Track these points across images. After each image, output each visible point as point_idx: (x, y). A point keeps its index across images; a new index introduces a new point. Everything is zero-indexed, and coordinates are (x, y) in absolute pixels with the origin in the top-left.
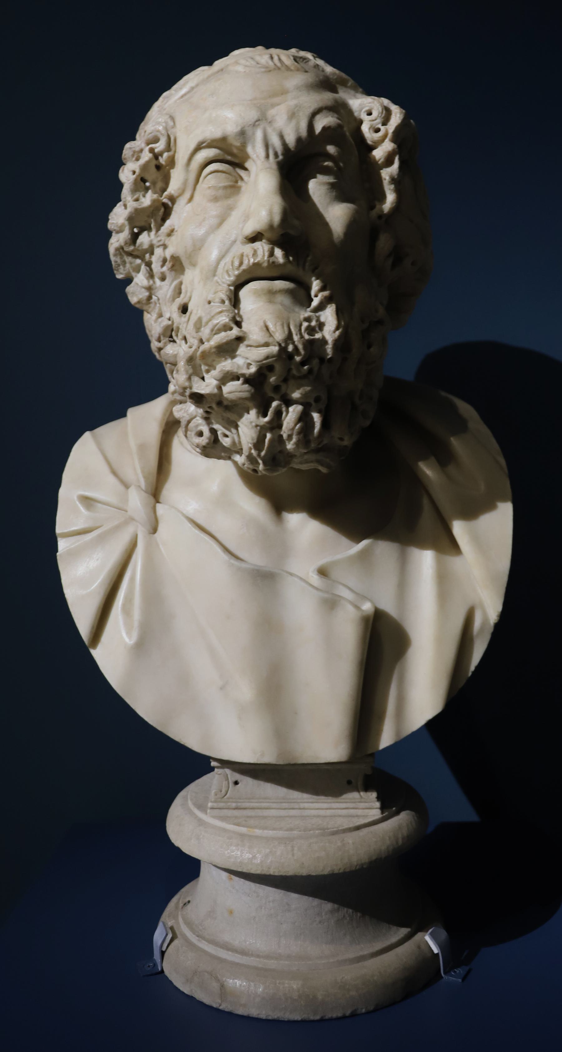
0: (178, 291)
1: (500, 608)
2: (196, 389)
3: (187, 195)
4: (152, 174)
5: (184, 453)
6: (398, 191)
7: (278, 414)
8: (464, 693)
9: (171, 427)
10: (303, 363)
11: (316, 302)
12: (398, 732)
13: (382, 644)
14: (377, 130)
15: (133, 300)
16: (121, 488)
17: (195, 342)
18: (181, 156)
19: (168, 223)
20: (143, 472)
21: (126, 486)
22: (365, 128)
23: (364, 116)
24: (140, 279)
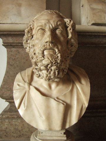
0: (34, 50)
1: (88, 105)
2: (36, 68)
3: (36, 34)
4: (30, 30)
5: (35, 77)
6: (72, 34)
7: (50, 72)
8: (82, 120)
9: (33, 73)
10: (54, 64)
11: (57, 53)
12: (70, 125)
13: (68, 108)
14: (69, 24)
15: (27, 51)
16: (24, 82)
17: (36, 60)
18: (35, 28)
19: (33, 39)
20: (28, 79)
21: (25, 82)
22: (67, 24)
23: (67, 22)
24: (28, 48)
